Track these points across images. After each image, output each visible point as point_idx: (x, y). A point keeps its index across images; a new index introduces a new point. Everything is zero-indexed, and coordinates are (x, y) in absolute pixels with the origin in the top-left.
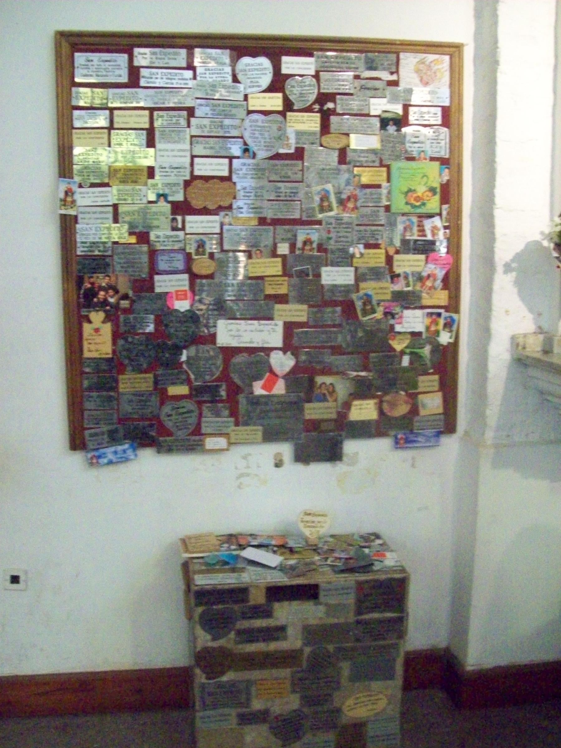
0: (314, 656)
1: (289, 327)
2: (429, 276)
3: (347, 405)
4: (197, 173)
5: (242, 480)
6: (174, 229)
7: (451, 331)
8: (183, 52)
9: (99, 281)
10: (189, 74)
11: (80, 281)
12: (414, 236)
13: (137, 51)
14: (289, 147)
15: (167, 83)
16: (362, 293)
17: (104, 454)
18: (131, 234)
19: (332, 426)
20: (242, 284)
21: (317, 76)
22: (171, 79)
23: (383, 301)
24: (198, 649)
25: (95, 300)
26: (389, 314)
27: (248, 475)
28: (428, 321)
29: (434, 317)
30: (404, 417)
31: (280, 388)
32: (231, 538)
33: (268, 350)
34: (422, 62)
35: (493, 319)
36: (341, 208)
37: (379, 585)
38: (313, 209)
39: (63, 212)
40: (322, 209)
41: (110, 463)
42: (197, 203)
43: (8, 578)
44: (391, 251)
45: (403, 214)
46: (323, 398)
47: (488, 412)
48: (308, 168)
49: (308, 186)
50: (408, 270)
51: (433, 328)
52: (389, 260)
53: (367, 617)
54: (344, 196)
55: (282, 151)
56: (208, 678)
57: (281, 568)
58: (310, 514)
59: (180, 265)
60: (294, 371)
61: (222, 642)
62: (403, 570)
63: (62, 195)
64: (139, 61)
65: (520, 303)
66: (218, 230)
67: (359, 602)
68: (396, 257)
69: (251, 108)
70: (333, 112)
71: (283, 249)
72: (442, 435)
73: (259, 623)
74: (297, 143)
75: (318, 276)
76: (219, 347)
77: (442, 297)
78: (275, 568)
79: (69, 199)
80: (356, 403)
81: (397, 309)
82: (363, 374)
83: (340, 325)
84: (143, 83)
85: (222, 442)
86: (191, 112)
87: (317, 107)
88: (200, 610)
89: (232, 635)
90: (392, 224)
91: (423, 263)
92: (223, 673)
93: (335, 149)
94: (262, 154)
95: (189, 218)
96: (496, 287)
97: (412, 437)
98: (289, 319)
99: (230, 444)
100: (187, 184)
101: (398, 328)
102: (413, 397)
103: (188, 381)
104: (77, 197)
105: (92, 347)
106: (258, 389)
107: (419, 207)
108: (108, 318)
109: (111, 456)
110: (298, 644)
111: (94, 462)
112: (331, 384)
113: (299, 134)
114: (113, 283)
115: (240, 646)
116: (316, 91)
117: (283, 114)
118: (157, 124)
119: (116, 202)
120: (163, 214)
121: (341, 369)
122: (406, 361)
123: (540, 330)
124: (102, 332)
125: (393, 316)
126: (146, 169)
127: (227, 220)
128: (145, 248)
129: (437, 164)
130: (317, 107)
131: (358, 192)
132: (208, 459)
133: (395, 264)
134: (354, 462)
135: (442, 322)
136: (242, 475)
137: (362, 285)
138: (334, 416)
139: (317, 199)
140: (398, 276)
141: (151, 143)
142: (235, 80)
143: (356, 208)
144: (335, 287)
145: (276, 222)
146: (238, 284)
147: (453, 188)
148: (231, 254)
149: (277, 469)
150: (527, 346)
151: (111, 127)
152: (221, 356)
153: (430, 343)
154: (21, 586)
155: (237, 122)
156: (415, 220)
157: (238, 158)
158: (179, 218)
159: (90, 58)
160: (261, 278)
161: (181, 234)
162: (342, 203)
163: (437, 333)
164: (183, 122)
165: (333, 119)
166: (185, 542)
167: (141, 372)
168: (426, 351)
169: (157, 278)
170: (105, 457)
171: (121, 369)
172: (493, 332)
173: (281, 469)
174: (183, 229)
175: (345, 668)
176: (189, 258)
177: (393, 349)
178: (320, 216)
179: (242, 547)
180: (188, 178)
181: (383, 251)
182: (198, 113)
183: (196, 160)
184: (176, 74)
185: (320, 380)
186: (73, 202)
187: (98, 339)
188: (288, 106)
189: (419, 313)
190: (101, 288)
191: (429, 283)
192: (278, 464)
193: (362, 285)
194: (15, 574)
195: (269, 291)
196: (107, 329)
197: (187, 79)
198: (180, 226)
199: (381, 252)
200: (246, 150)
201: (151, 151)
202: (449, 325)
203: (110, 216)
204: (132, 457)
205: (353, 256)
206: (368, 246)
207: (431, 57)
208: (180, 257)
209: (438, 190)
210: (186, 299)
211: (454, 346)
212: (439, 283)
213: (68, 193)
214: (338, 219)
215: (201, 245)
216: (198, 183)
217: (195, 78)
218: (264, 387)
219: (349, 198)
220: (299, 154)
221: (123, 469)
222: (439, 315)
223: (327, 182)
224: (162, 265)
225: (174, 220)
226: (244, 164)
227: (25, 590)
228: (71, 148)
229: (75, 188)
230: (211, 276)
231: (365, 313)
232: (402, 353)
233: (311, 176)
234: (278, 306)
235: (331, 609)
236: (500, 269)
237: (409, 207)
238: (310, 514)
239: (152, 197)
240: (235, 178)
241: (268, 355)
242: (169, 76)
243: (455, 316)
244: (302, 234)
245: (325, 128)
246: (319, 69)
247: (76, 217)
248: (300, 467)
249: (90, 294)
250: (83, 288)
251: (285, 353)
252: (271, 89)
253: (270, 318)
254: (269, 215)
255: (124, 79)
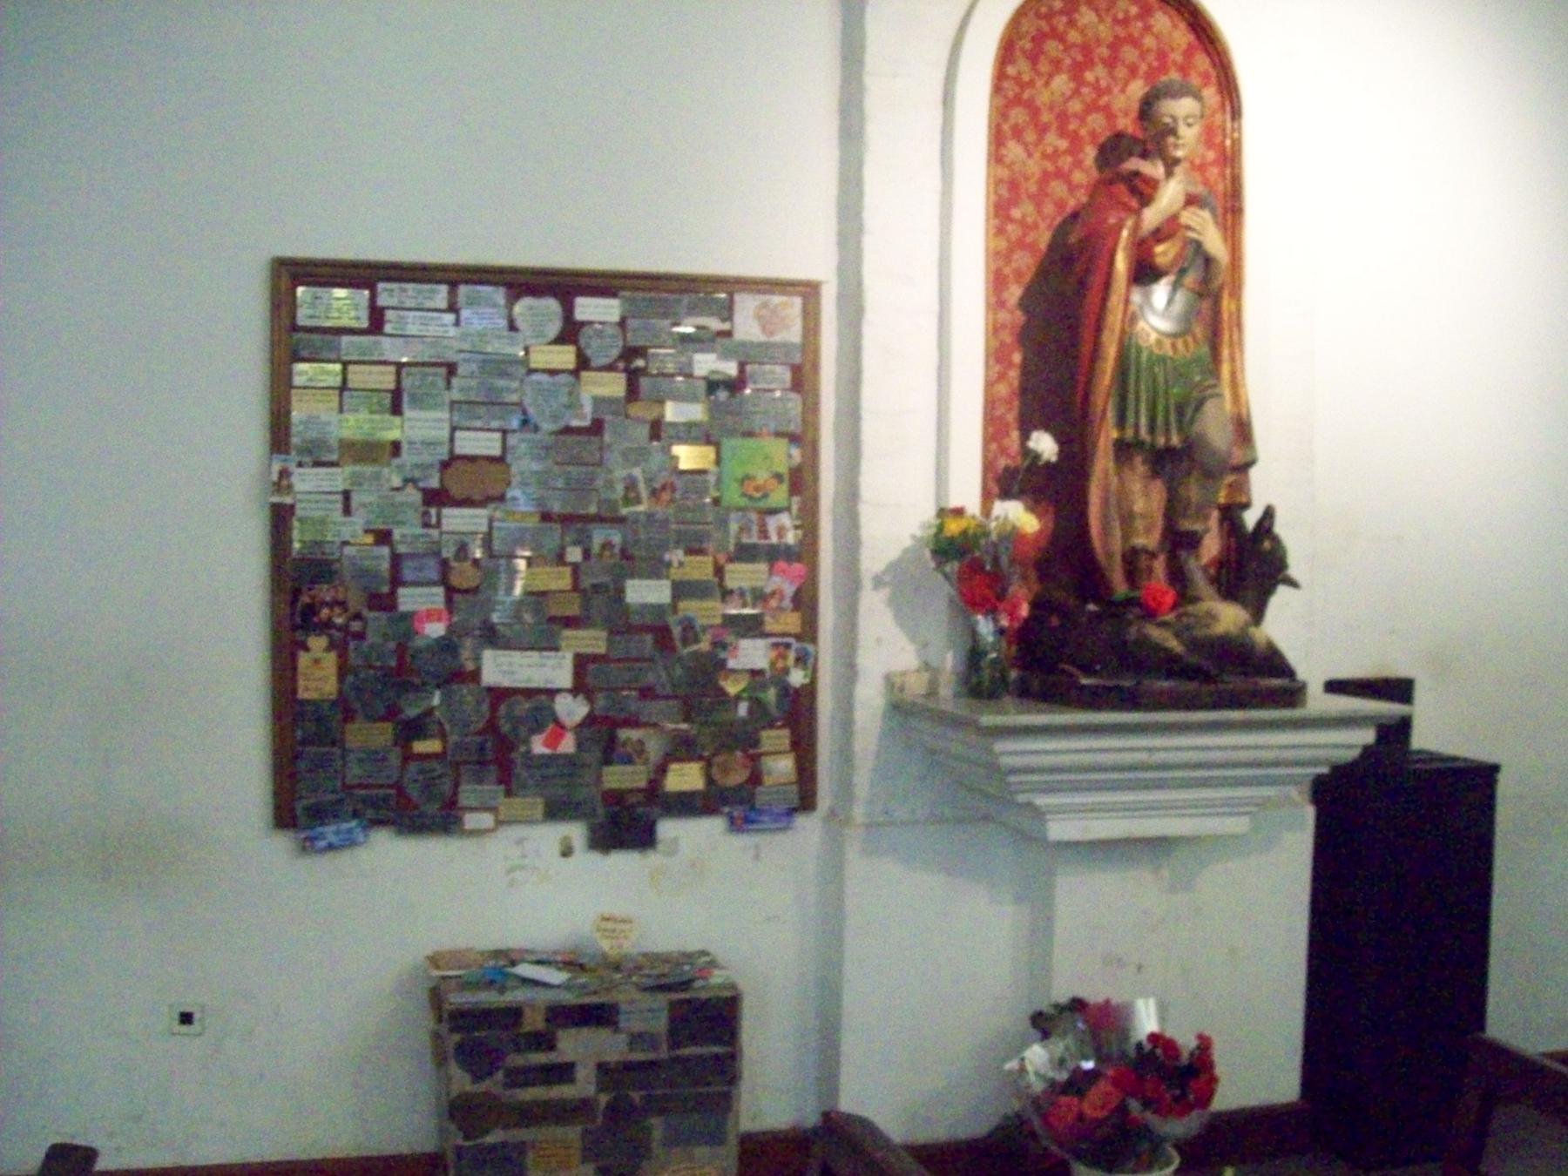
0: (612, 1108)
1: (582, 663)
2: (773, 593)
3: (662, 770)
4: (459, 451)
5: (512, 875)
6: (426, 525)
7: (805, 669)
8: (444, 289)
9: (322, 595)
10: (450, 318)
11: (296, 593)
12: (753, 539)
13: (381, 286)
14: (583, 417)
15: (421, 331)
16: (681, 614)
17: (322, 833)
18: (367, 531)
19: (640, 797)
20: (520, 604)
21: (622, 324)
22: (426, 325)
23: (711, 626)
24: (454, 1094)
25: (315, 619)
26: (719, 644)
27: (522, 868)
28: (773, 654)
29: (782, 649)
30: (740, 787)
31: (568, 745)
32: (497, 954)
33: (552, 693)
34: (765, 305)
35: (860, 652)
36: (653, 499)
37: (698, 1006)
38: (616, 501)
39: (276, 499)
40: (628, 501)
41: (331, 847)
42: (456, 491)
43: (176, 1016)
44: (722, 559)
45: (739, 509)
46: (629, 760)
47: (856, 779)
48: (610, 446)
49: (610, 471)
50: (746, 585)
51: (780, 664)
52: (719, 571)
53: (687, 1051)
54: (657, 485)
55: (575, 423)
56: (467, 1137)
57: (566, 987)
58: (608, 919)
59: (434, 575)
60: (590, 720)
61: (481, 1087)
62: (733, 986)
63: (275, 477)
64: (383, 300)
65: (896, 630)
66: (484, 528)
67: (673, 1032)
68: (730, 567)
69: (533, 365)
70: (643, 372)
71: (575, 554)
72: (796, 815)
73: (539, 1058)
74: (594, 412)
75: (620, 591)
76: (485, 688)
77: (791, 622)
78: (559, 986)
79: (284, 482)
80: (674, 766)
81: (729, 639)
82: (684, 726)
83: (651, 660)
84: (388, 328)
85: (486, 820)
86: (451, 369)
87: (621, 365)
88: (457, 1037)
89: (500, 1075)
90: (723, 523)
91: (765, 576)
92: (487, 1132)
93: (645, 422)
94: (547, 426)
95: (446, 511)
96: (863, 607)
97: (753, 815)
98: (583, 650)
99: (499, 823)
100: (445, 465)
101: (732, 664)
102: (755, 759)
103: (443, 736)
104: (295, 480)
105: (312, 685)
106: (538, 746)
107: (759, 499)
108: (331, 646)
109: (333, 839)
110: (590, 1090)
111: (308, 846)
112: (639, 741)
113: (598, 401)
114: (341, 597)
115: (508, 1093)
116: (621, 343)
117: (575, 373)
118: (407, 383)
119: (348, 487)
120: (411, 505)
121: (654, 719)
122: (743, 709)
123: (927, 666)
124: (324, 664)
125: (724, 646)
126: (388, 445)
127: (498, 514)
128: (385, 551)
129: (784, 442)
130: (621, 365)
131: (674, 479)
132: (470, 844)
133: (727, 576)
134: (673, 851)
135: (792, 656)
136: (510, 870)
137: (682, 605)
138: (643, 784)
139: (620, 488)
140: (731, 592)
141: (396, 409)
142: (512, 327)
143: (672, 501)
144: (645, 606)
145: (567, 520)
146: (512, 603)
147: (807, 477)
148: (503, 562)
149: (565, 859)
150: (907, 686)
151: (343, 388)
152: (488, 700)
153: (776, 685)
154: (195, 1028)
155: (515, 385)
156: (754, 516)
157: (514, 431)
158: (433, 511)
159: (319, 295)
160: (543, 594)
161: (434, 533)
162: (654, 493)
163: (786, 671)
164: (441, 383)
165: (644, 382)
166: (435, 960)
167: (375, 721)
168: (771, 695)
169: (402, 591)
170: (324, 838)
171: (349, 716)
172: (859, 668)
173: (570, 860)
174: (438, 524)
175: (657, 1127)
176: (444, 564)
177: (722, 692)
178: (624, 511)
179: (513, 964)
180: (445, 457)
181: (710, 559)
182: (461, 370)
183: (458, 434)
184: (432, 318)
185: (625, 734)
186: (290, 487)
187: (318, 674)
188: (583, 363)
189: (761, 643)
190: (324, 604)
191: (774, 603)
192: (567, 852)
193: (682, 605)
194: (188, 1009)
195: (555, 610)
196: (330, 660)
197: (446, 325)
198: (434, 520)
199: (709, 560)
200: (525, 422)
201: (397, 420)
202: (801, 660)
203: (339, 506)
204: (361, 838)
205: (669, 565)
206: (690, 551)
207: (776, 299)
208: (432, 563)
209: (786, 477)
210: (439, 620)
211: (810, 690)
212: (787, 603)
213: (284, 473)
214: (650, 516)
215: (462, 550)
216: (458, 464)
217: (457, 323)
218: (546, 744)
219: (664, 488)
220: (597, 427)
221: (344, 859)
222: (788, 646)
223: (636, 463)
224: (408, 573)
225: (426, 514)
226: (523, 441)
227: (200, 1034)
228: (288, 413)
229: (292, 467)
230: (474, 591)
231: (686, 641)
232: (738, 698)
233: (614, 458)
234: (567, 633)
235: (637, 1039)
236: (867, 583)
237: (745, 499)
238: (608, 919)
239: (396, 481)
240: (509, 458)
241: (553, 700)
242: (423, 321)
243: (810, 648)
244: (599, 536)
245: (633, 392)
246: (627, 314)
247: (292, 507)
248: (596, 857)
249: (311, 610)
250: (299, 604)
251: (575, 696)
252: (561, 340)
253: (556, 649)
254: (556, 507)
255: (365, 324)
